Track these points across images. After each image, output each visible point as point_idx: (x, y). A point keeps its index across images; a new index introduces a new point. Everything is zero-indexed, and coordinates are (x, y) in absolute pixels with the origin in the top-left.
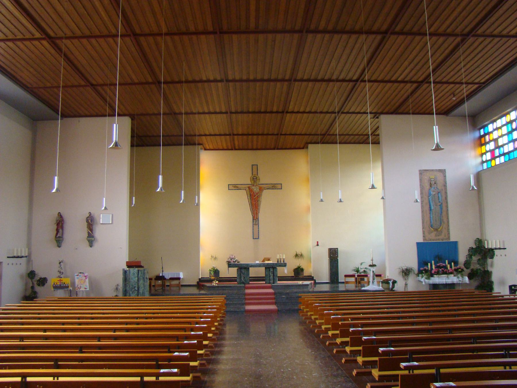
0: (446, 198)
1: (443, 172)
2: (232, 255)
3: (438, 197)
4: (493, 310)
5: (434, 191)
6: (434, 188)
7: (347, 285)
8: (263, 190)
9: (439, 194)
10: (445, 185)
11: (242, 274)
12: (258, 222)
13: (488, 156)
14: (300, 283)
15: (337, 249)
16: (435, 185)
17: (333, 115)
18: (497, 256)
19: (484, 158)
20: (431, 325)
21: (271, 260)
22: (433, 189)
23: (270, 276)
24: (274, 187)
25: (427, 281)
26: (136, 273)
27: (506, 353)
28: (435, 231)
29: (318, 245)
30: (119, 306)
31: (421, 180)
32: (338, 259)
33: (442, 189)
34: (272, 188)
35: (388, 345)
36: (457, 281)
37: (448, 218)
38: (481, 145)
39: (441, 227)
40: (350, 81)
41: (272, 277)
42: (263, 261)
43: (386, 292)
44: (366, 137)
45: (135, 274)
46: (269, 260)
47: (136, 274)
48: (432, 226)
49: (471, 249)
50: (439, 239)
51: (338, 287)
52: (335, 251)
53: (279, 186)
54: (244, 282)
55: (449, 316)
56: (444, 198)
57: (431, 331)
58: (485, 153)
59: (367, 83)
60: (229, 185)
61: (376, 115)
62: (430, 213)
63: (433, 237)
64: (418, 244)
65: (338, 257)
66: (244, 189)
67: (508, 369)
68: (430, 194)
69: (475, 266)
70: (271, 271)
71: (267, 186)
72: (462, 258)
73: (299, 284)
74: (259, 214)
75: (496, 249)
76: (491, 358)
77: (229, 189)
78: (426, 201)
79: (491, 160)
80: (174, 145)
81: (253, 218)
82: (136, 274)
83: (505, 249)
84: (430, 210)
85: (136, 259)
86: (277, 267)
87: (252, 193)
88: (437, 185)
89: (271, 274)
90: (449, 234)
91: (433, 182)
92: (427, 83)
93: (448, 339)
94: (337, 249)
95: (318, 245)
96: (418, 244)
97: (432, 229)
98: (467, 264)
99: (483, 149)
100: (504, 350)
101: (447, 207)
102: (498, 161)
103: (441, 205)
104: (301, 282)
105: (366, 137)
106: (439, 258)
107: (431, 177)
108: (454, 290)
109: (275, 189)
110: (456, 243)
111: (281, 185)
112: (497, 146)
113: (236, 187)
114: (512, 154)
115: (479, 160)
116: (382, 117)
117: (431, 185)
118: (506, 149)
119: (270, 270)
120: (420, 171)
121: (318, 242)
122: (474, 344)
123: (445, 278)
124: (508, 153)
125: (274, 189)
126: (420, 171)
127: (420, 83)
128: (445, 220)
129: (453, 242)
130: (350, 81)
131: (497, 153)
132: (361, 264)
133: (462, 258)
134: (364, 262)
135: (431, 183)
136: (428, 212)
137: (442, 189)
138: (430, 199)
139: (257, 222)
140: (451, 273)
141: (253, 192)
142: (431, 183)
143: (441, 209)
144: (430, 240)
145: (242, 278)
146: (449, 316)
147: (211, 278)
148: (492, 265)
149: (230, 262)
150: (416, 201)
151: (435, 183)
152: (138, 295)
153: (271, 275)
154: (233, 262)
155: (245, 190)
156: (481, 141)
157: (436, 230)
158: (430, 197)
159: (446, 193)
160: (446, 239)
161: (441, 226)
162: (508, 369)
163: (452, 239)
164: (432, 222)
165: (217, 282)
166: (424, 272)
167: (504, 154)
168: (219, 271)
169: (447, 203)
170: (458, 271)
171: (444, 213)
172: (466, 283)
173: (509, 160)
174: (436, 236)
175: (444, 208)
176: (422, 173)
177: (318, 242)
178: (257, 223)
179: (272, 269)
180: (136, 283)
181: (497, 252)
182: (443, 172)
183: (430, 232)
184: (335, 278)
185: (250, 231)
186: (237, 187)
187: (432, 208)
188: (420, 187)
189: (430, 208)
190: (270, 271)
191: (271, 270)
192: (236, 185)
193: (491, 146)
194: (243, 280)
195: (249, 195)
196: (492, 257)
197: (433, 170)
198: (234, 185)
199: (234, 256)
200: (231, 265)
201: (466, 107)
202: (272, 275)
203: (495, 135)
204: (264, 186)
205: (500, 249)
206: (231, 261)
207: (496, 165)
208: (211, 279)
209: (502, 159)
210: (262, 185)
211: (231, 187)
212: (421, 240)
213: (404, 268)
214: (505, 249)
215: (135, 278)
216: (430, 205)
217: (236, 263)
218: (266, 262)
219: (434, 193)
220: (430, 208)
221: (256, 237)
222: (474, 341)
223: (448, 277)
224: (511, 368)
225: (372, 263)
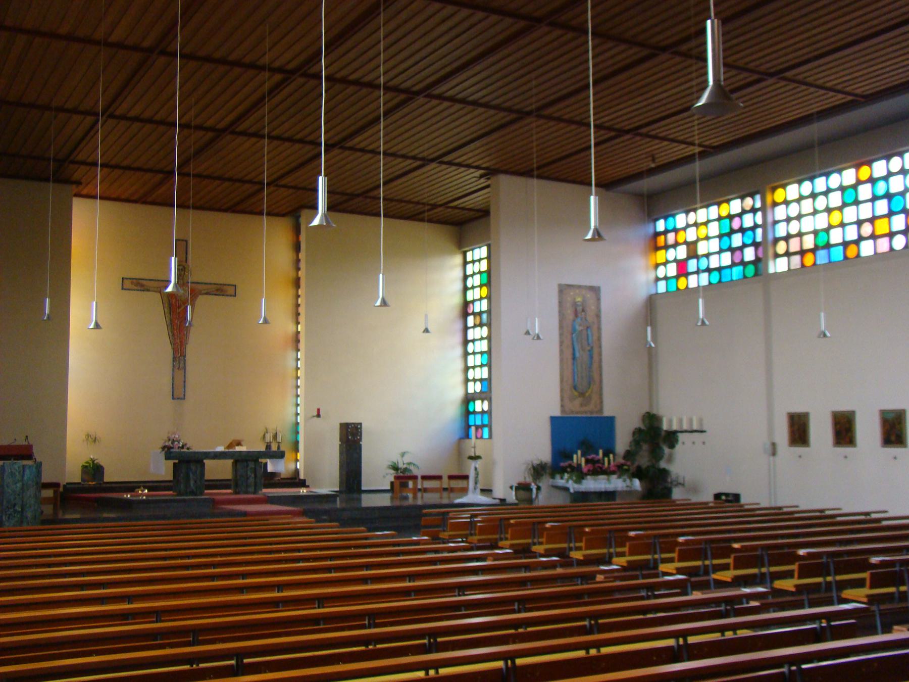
0: (599, 339)
1: (596, 290)
2: (174, 433)
3: (588, 335)
4: (192, 570)
5: (580, 325)
6: (581, 319)
7: (426, 495)
8: (198, 296)
9: (589, 330)
10: (598, 316)
11: (191, 475)
12: (185, 364)
13: (672, 270)
14: (303, 492)
15: (361, 424)
16: (583, 313)
17: (89, 120)
18: (683, 443)
19: (661, 272)
20: (282, 592)
21: (242, 443)
22: (579, 320)
23: (248, 478)
24: (220, 290)
25: (576, 486)
26: (19, 472)
27: (590, 623)
28: (579, 396)
29: (318, 415)
30: (107, 539)
31: (561, 304)
32: (361, 445)
33: (593, 323)
34: (215, 293)
35: (191, 639)
36: (622, 487)
37: (601, 375)
38: (657, 248)
39: (590, 390)
40: (135, 48)
41: (253, 479)
42: (230, 446)
43: (522, 506)
44: (257, 187)
45: (15, 473)
46: (239, 444)
47: (17, 474)
48: (575, 388)
49: (638, 432)
50: (586, 412)
51: (360, 500)
52: (357, 428)
53: (230, 290)
54: (195, 490)
55: (212, 577)
56: (595, 338)
57: (413, 594)
58: (665, 264)
59: (102, 47)
60: (123, 279)
61: (490, 172)
62: (573, 364)
63: (576, 408)
64: (553, 419)
65: (360, 440)
66: (155, 289)
67: (593, 652)
68: (574, 330)
69: (643, 460)
70: (251, 468)
71: (205, 287)
72: (622, 442)
73: (301, 494)
74: (187, 345)
75: (682, 432)
76: (453, 649)
77: (122, 289)
78: (567, 342)
79: (677, 277)
80: (27, 177)
81: (174, 354)
82: (17, 474)
83: (705, 431)
84: (574, 358)
85: (15, 440)
86: (205, 461)
87: (174, 301)
88: (586, 314)
89: (249, 473)
90: (601, 402)
91: (579, 309)
92: (163, 53)
93: (456, 606)
94: (361, 424)
95: (318, 415)
96: (553, 419)
97: (576, 393)
98: (628, 455)
99: (661, 256)
100: (427, 638)
101: (600, 354)
102: (693, 282)
103: (591, 351)
104: (305, 491)
105: (257, 187)
106: (587, 447)
107: (579, 299)
108: (613, 502)
109: (223, 295)
110: (611, 420)
111: (234, 287)
112: (692, 254)
113: (137, 285)
114: (726, 272)
115: (652, 276)
116: (506, 183)
117: (576, 314)
118: (714, 262)
119: (247, 466)
120: (560, 286)
121: (319, 410)
122: (370, 627)
123: (604, 481)
124: (720, 269)
125: (220, 295)
126: (560, 286)
127: (288, 74)
128: (596, 377)
129: (607, 417)
130: (135, 48)
131: (692, 265)
132: (403, 455)
133: (622, 442)
134: (408, 452)
135: (576, 310)
136: (570, 361)
137: (593, 323)
138: (575, 339)
139: (182, 362)
140: (613, 473)
141: (176, 299)
142: (576, 310)
143: (591, 357)
144: (572, 412)
145: (192, 483)
146: (212, 577)
147: (86, 483)
148: (670, 460)
149: (173, 448)
150: (536, 337)
151: (583, 311)
152: (22, 522)
153: (250, 476)
154: (179, 447)
155: (159, 294)
156: (656, 242)
157: (582, 394)
158: (574, 335)
159: (599, 329)
160: (597, 412)
161: (589, 388)
162: (729, 635)
163: (607, 412)
164: (576, 380)
165: (146, 491)
166: (569, 470)
167: (709, 270)
168: (104, 469)
169: (600, 347)
170: (620, 470)
171: (595, 365)
172: (637, 491)
173: (720, 281)
174: (582, 405)
175: (596, 357)
176: (563, 289)
177: (319, 410)
178: (182, 365)
179: (253, 463)
180: (19, 495)
181: (681, 437)
182: (596, 290)
183: (572, 399)
184: (356, 482)
185: (167, 380)
186: (142, 285)
187: (577, 355)
188: (560, 315)
189: (574, 354)
190: (249, 468)
191: (252, 465)
192: (141, 281)
193: (681, 252)
194: (192, 485)
195: (167, 305)
196: (672, 446)
197: (580, 287)
198: (134, 281)
199: (179, 436)
200: (172, 455)
201: (646, 184)
202: (253, 475)
203: (691, 235)
204: (200, 287)
205: (686, 431)
206: (171, 445)
207: (687, 287)
208: (85, 486)
209: (704, 279)
210: (195, 284)
211: (128, 284)
212: (557, 413)
213: (536, 462)
214: (705, 431)
215: (16, 483)
216: (574, 349)
217: (185, 450)
218: (238, 449)
219: (581, 328)
220: (574, 354)
221: (178, 394)
222: (371, 622)
223: (608, 480)
224: (735, 634)
225: (475, 454)
